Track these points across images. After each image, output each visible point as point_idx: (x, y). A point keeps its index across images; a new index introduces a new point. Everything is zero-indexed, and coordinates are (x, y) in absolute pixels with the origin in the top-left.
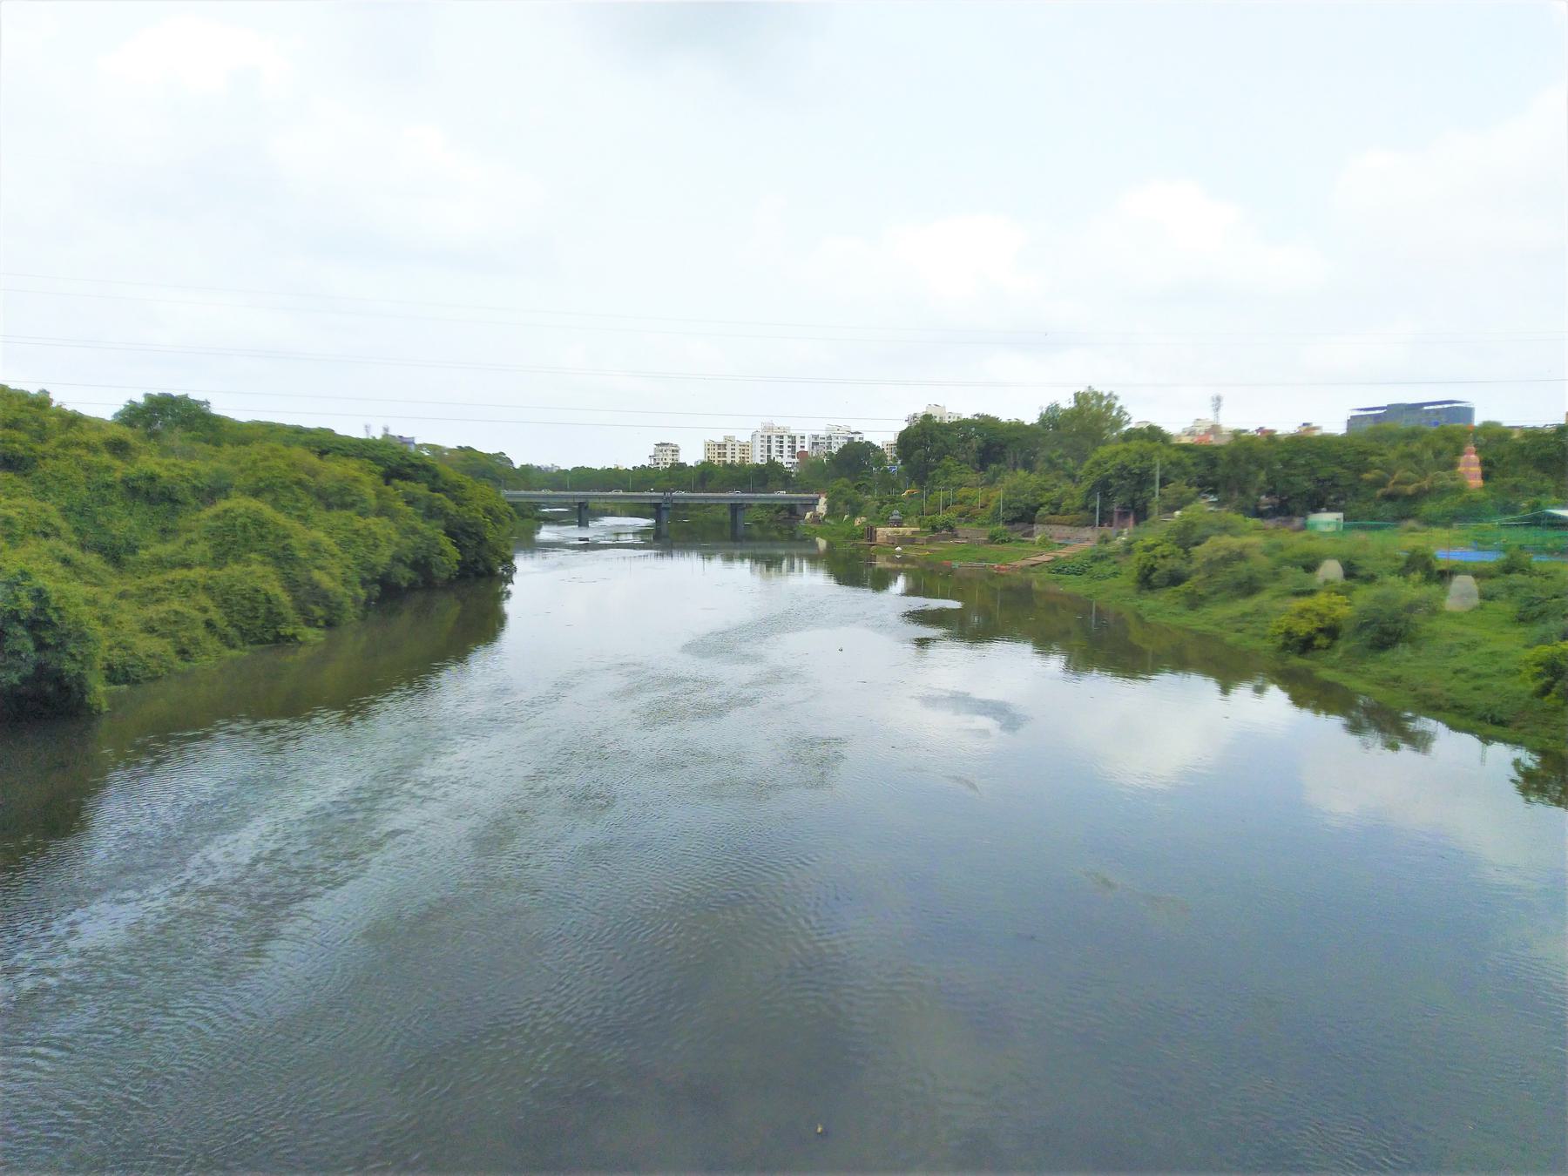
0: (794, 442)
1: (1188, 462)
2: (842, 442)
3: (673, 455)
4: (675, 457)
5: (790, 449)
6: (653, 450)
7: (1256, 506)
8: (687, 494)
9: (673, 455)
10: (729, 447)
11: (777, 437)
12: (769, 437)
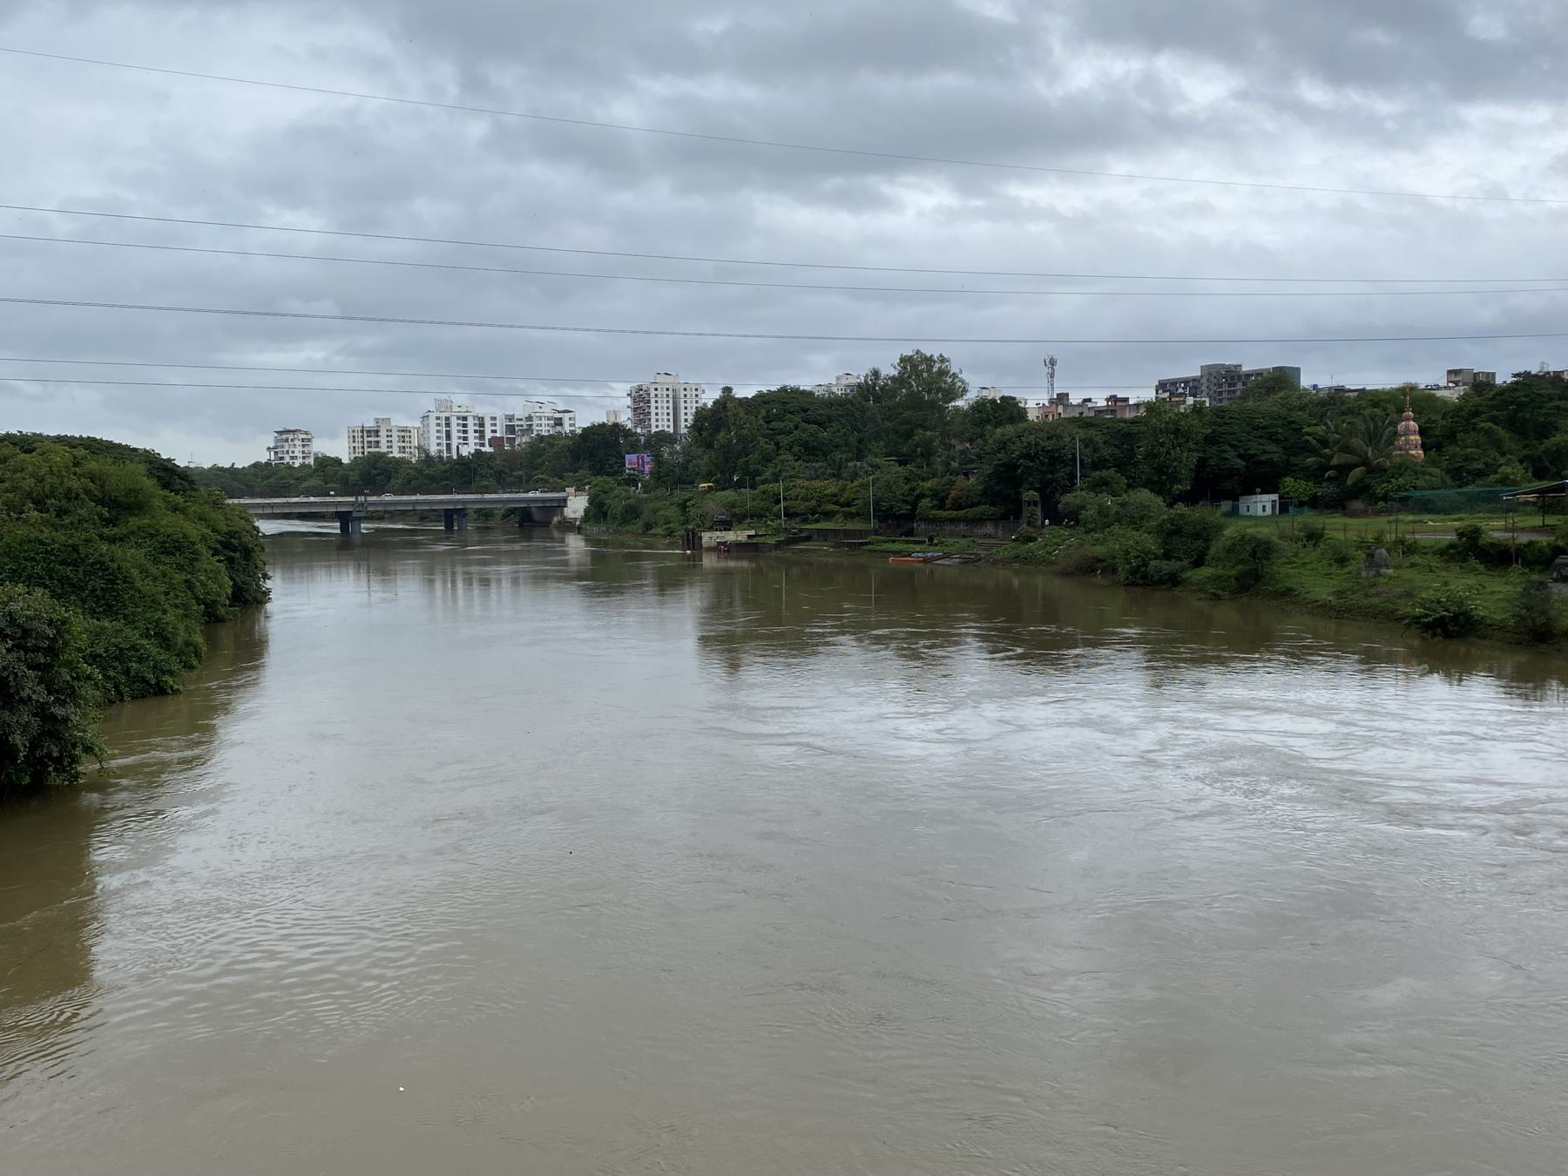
0: (482, 425)
1: (1099, 439)
2: (854, 520)
3: (304, 446)
4: (306, 449)
5: (477, 435)
6: (273, 439)
7: (1118, 504)
8: (542, 495)
9: (304, 446)
10: (383, 433)
11: (458, 418)
12: (447, 419)
